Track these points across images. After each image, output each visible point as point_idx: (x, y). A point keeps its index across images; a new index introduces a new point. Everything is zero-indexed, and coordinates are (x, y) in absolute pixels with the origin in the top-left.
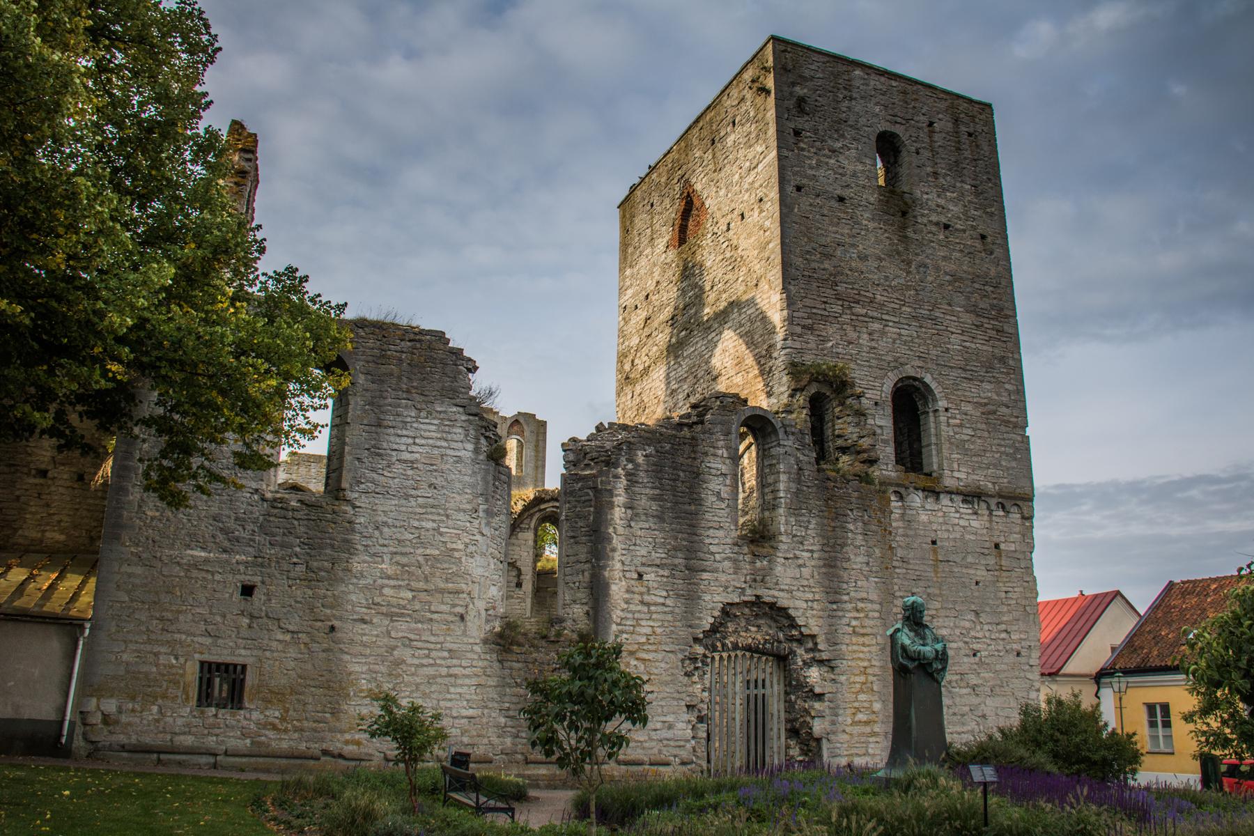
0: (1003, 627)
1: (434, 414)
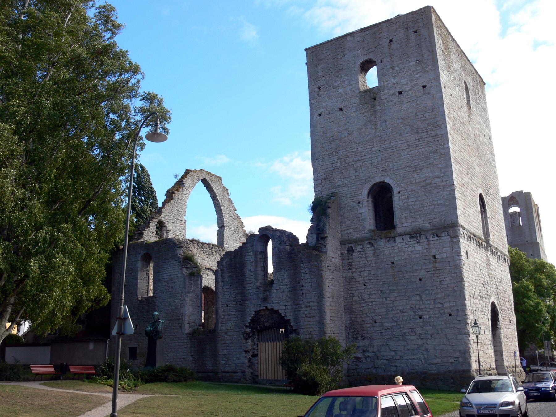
0: (438, 301)
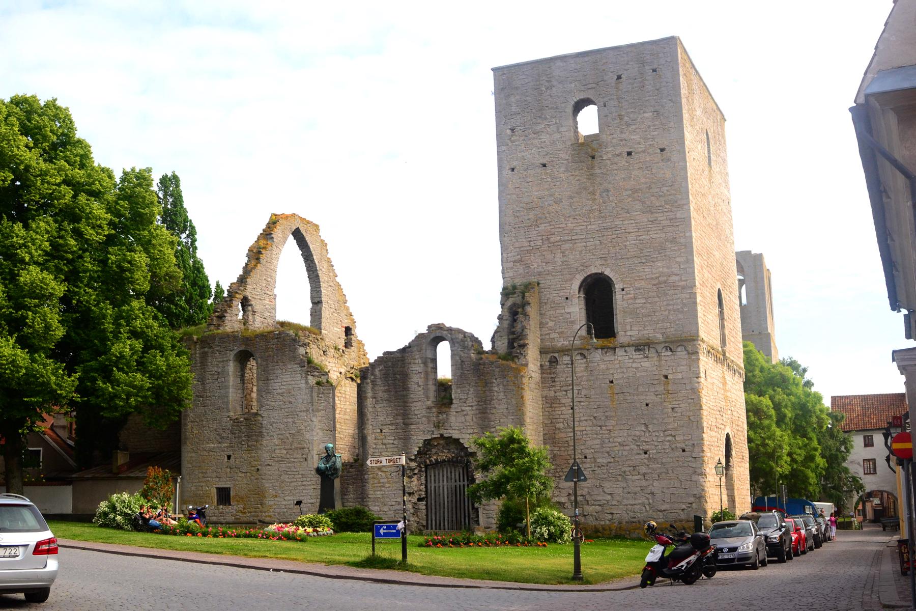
0: (670, 432)
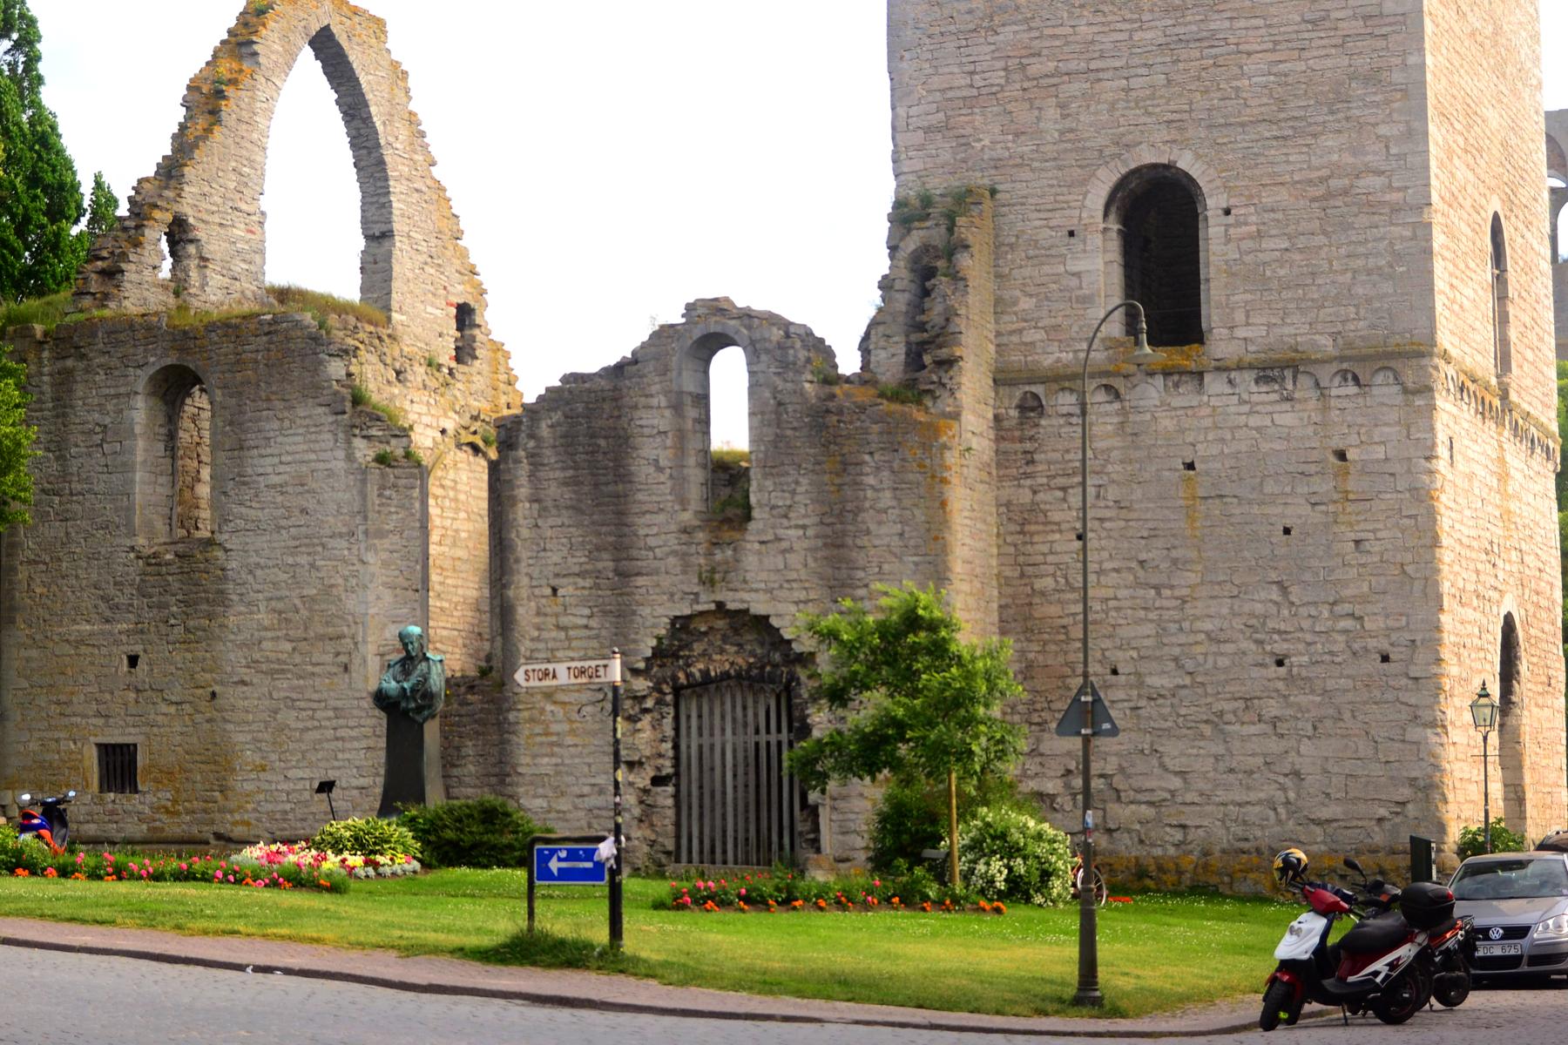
1: (298, 421)
